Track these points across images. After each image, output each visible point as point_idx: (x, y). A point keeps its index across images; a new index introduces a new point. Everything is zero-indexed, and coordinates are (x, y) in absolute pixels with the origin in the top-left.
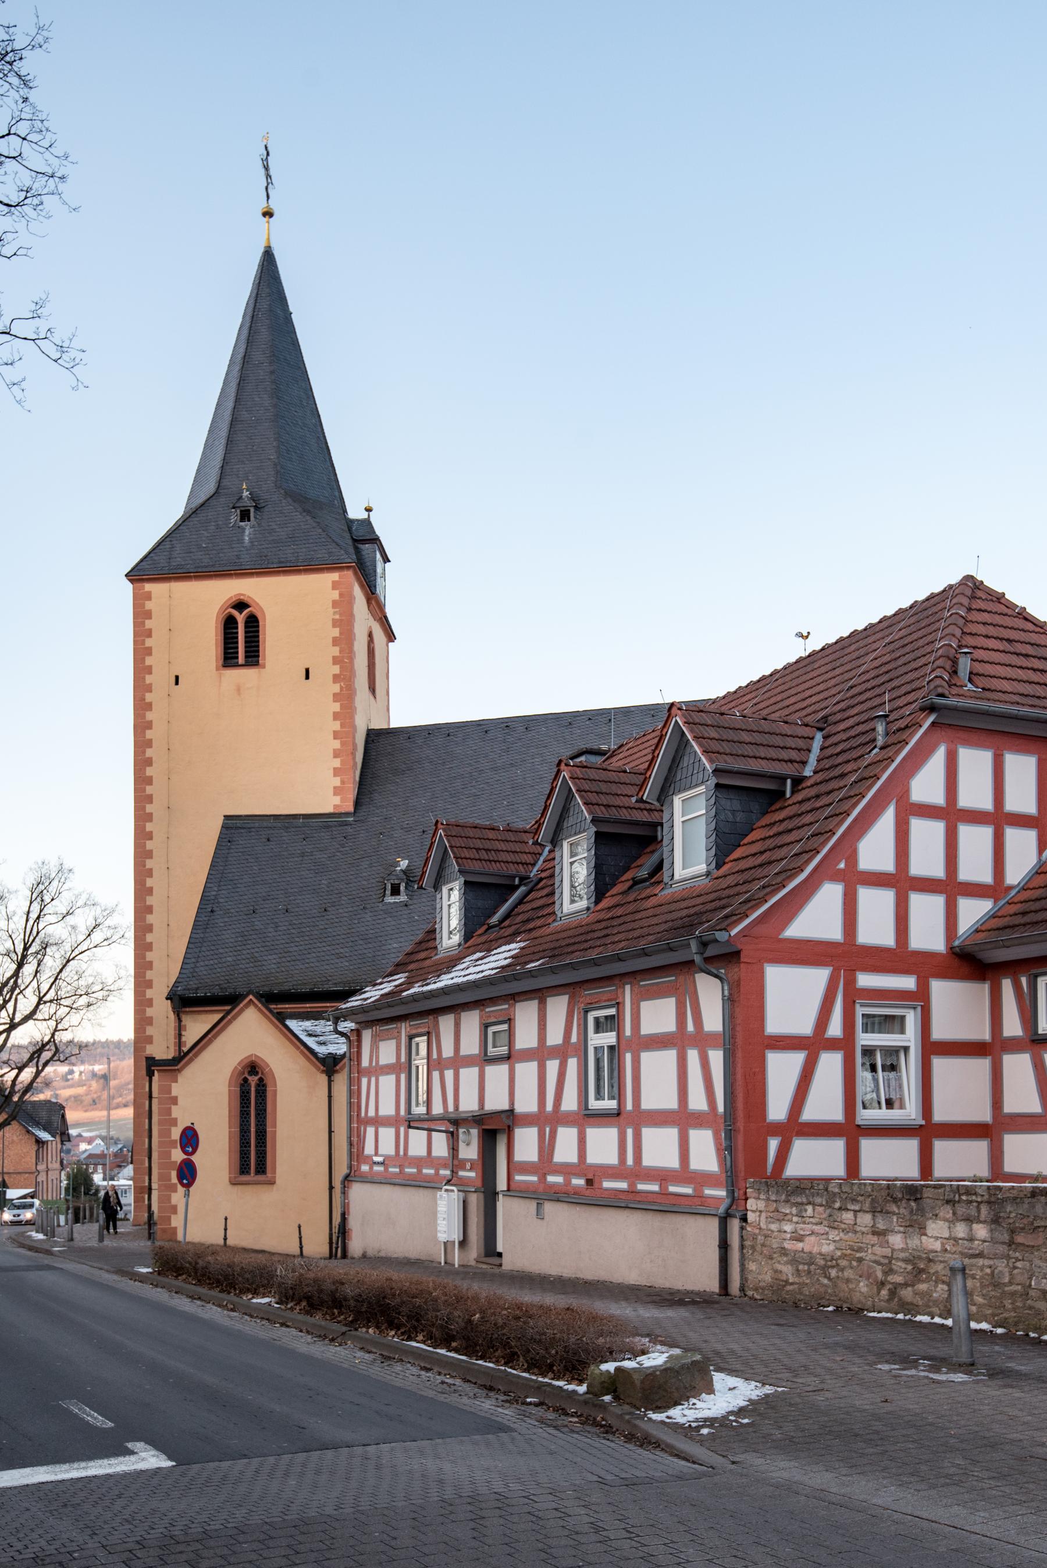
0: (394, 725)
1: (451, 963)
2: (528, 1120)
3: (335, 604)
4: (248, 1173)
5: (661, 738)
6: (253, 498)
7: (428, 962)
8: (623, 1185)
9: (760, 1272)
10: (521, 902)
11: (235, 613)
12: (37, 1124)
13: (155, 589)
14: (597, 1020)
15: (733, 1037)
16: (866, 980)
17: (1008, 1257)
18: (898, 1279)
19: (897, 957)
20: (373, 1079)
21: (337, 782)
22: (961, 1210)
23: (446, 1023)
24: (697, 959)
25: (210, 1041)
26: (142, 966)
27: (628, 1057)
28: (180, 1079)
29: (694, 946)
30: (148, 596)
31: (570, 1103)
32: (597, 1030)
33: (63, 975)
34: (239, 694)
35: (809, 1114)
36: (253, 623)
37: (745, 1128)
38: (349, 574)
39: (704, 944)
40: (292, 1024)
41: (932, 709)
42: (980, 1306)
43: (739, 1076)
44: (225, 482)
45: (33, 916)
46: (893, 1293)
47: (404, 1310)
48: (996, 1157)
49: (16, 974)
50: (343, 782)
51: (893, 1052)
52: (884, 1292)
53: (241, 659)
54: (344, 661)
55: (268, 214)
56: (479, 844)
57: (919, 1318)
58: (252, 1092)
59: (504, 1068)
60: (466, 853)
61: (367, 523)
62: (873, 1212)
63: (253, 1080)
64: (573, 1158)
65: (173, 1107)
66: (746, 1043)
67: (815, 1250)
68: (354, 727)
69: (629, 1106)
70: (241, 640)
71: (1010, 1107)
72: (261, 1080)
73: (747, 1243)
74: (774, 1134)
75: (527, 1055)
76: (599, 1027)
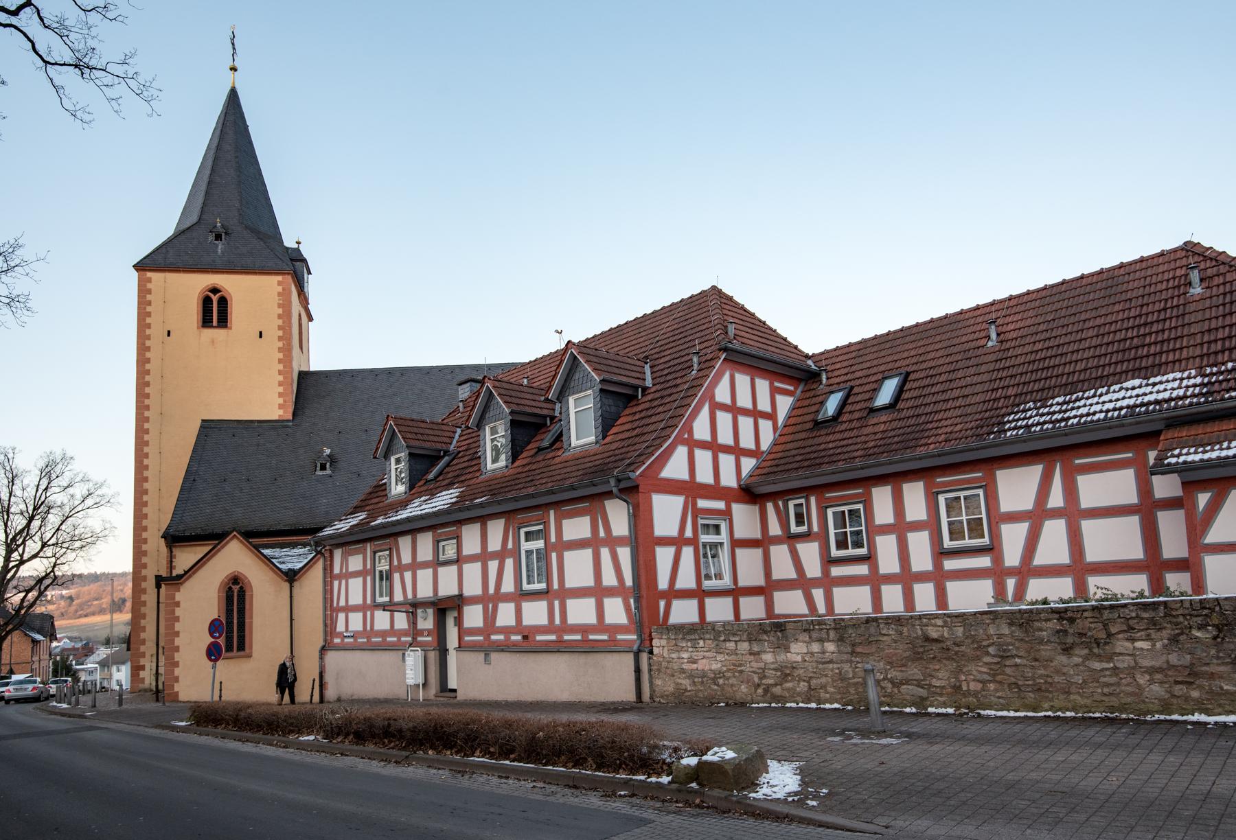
0: (312, 369)
1: (403, 503)
2: (474, 600)
3: (279, 294)
4: (232, 650)
5: (562, 361)
6: (223, 226)
7: (381, 505)
8: (553, 637)
9: (665, 685)
10: (448, 465)
11: (211, 295)
12: (33, 629)
13: (155, 276)
14: (527, 534)
15: (636, 538)
16: (702, 503)
17: (851, 662)
18: (771, 681)
19: (715, 491)
20: (344, 582)
21: (281, 401)
22: (815, 635)
23: (405, 543)
24: (615, 490)
25: (205, 563)
26: (139, 517)
27: (554, 555)
29: (613, 482)
30: (150, 280)
31: (508, 586)
32: (527, 540)
33: (63, 527)
35: (1040, 560)
36: (223, 302)
37: (645, 595)
38: (289, 277)
39: (619, 481)
40: (266, 552)
41: (725, 349)
42: (832, 693)
43: (641, 562)
44: (204, 217)
45: (43, 487)
46: (766, 691)
47: (461, 735)
48: (769, 605)
49: (28, 525)
51: (714, 546)
52: (760, 691)
53: (215, 323)
54: (285, 328)
55: (234, 69)
56: (416, 430)
57: (788, 705)
58: (236, 595)
59: (454, 569)
60: (409, 435)
61: (298, 250)
62: (750, 641)
63: (236, 588)
64: (512, 623)
66: (643, 542)
67: (707, 668)
68: (292, 368)
69: (556, 586)
70: (215, 311)
71: (776, 575)
72: (241, 588)
73: (654, 668)
74: (662, 598)
75: (472, 559)
76: (529, 536)
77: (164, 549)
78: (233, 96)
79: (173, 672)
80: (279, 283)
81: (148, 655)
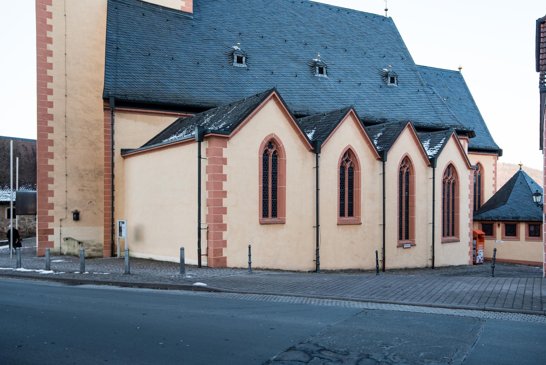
65: (224, 166)
79: (221, 235)
81: (56, 220)
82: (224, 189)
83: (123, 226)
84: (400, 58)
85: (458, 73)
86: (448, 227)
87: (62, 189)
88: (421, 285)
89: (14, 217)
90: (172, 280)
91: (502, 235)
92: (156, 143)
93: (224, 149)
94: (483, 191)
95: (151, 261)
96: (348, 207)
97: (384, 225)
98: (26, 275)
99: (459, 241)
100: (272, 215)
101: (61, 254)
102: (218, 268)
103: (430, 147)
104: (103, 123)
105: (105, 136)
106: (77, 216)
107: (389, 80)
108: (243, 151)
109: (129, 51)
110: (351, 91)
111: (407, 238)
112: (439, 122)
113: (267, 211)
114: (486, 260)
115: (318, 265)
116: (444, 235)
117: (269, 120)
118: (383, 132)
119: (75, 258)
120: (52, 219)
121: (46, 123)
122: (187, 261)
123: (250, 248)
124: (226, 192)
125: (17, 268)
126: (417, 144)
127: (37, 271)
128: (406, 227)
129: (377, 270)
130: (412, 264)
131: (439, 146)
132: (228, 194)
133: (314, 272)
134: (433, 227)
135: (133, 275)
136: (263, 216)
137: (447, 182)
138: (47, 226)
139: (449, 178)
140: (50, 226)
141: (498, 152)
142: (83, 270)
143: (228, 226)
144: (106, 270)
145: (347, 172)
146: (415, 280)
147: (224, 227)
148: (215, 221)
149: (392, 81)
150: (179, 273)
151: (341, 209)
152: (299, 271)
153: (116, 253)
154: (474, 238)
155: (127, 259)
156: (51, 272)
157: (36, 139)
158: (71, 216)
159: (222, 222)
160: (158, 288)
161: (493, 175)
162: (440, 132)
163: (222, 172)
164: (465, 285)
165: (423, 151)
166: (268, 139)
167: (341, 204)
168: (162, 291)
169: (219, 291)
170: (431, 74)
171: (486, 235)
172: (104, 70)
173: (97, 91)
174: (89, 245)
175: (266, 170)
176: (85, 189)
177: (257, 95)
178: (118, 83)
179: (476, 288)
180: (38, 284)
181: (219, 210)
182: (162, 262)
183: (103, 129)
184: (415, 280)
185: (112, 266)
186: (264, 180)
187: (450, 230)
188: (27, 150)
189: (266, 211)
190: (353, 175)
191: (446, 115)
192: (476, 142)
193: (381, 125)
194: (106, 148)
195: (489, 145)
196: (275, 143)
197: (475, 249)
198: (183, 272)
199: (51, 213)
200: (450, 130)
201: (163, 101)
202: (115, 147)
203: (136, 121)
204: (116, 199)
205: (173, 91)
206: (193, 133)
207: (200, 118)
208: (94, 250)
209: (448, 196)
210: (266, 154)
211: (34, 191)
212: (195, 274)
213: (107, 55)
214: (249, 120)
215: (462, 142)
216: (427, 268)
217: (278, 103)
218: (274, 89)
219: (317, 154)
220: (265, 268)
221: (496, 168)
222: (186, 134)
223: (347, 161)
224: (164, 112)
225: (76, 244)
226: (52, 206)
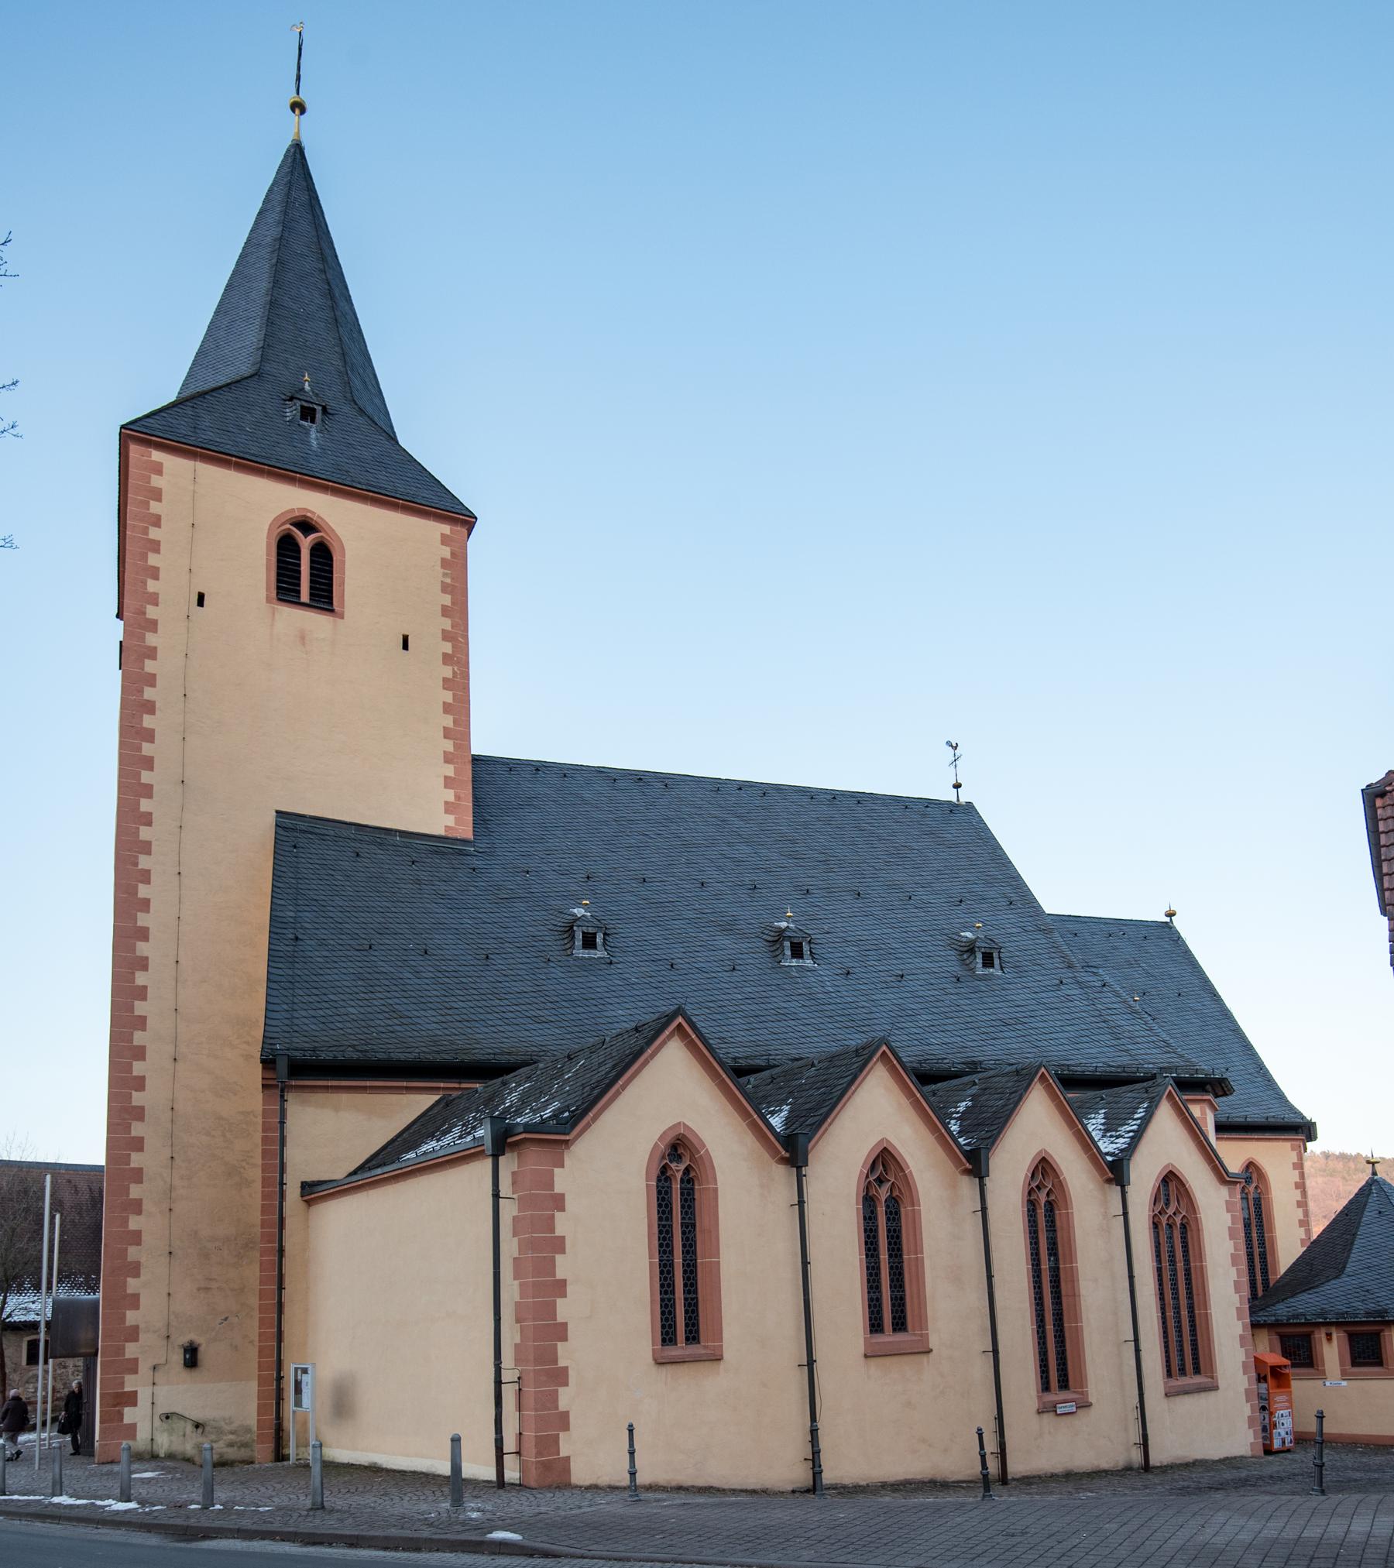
13: (175, 472)
21: (450, 795)
28: (567, 1161)
34: (304, 644)
36: (323, 555)
50: (457, 797)
53: (305, 596)
55: (298, 107)
70: (304, 571)
77: (254, 1099)
78: (296, 157)
79: (554, 1398)
80: (445, 540)
81: (144, 1367)
82: (560, 1275)
83: (306, 1379)
84: (1004, 902)
85: (1168, 927)
86: (1181, 1350)
87: (157, 1293)
88: (1114, 1526)
89: (46, 1362)
90: (431, 1525)
91: (1342, 1364)
92: (384, 1165)
93: (557, 1171)
94: (1273, 1240)
95: (374, 1470)
96: (892, 1306)
97: (995, 1351)
98: (74, 1513)
99: (1215, 1388)
100: (687, 1339)
101: (154, 1457)
102: (549, 1487)
103: (1107, 1130)
104: (260, 1120)
105: (265, 1153)
106: (192, 1357)
107: (979, 960)
108: (605, 1176)
109: (322, 943)
110: (878, 997)
111: (1064, 1384)
112: (1125, 1060)
113: (673, 1326)
114: (1301, 1439)
115: (817, 1473)
116: (1169, 1374)
117: (672, 1091)
118: (974, 1098)
119: (186, 1466)
120: (133, 1367)
121: (128, 1128)
122: (469, 1470)
123: (631, 1431)
124: (563, 1283)
125: (54, 1495)
126: (1071, 1124)
127: (99, 1503)
128: (1058, 1353)
129: (986, 1482)
130: (1084, 1459)
131: (1133, 1126)
132: (569, 1289)
133: (808, 1491)
134: (1137, 1351)
135: (332, 1511)
136: (664, 1341)
137: (1164, 1222)
138: (122, 1384)
139: (1170, 1211)
140: (130, 1384)
141: (1304, 1130)
142: (208, 1501)
143: (570, 1372)
144: (266, 1500)
145: (881, 1210)
146: (1096, 1512)
147: (561, 1377)
148: (538, 1361)
149: (988, 961)
150: (447, 1505)
151: (871, 1313)
152: (765, 1491)
153: (286, 1451)
154: (1261, 1378)
155: (316, 1469)
156: (133, 1505)
157: (103, 1163)
158: (178, 1357)
159: (556, 1361)
160: (396, 1549)
161: (1297, 1195)
162: (1131, 1087)
163: (553, 1230)
164: (1242, 1522)
165: (1087, 1144)
166: (668, 1139)
167: (871, 1300)
168: (406, 1555)
169: (555, 1556)
170: (1093, 934)
171: (1294, 1365)
172: (263, 990)
173: (247, 1043)
174: (220, 1431)
175: (667, 1219)
176: (214, 1285)
177: (636, 1029)
178: (296, 1021)
179: (1271, 1530)
180: (104, 1538)
181: (547, 1332)
182: (402, 1473)
183: (258, 1136)
184: (1096, 1512)
185: (279, 1486)
186: (661, 1246)
187: (1187, 1356)
188: (77, 1192)
189: (670, 1326)
190: (899, 1219)
191: (1147, 1036)
192: (1236, 1107)
193: (966, 1079)
194: (265, 1182)
195: (1275, 1114)
196: (685, 1147)
197: (1265, 1408)
198: (458, 1501)
199: (131, 1350)
200: (1159, 1080)
201: (402, 1057)
202: (287, 1178)
203: (337, 1109)
204: (287, 1309)
205: (427, 1033)
206: (480, 1133)
207: (495, 1093)
208: (231, 1445)
209: (1173, 1261)
210: (663, 1176)
211: (92, 1296)
212: (489, 1508)
213: (273, 956)
214: (618, 1094)
215: (1196, 1110)
216: (1128, 1469)
217: (691, 1046)
218: (679, 1011)
219: (799, 1168)
220: (674, 1484)
221: (1302, 1175)
222: (460, 1137)
223: (880, 1181)
224: (405, 1084)
225: (189, 1428)
226: (133, 1334)
